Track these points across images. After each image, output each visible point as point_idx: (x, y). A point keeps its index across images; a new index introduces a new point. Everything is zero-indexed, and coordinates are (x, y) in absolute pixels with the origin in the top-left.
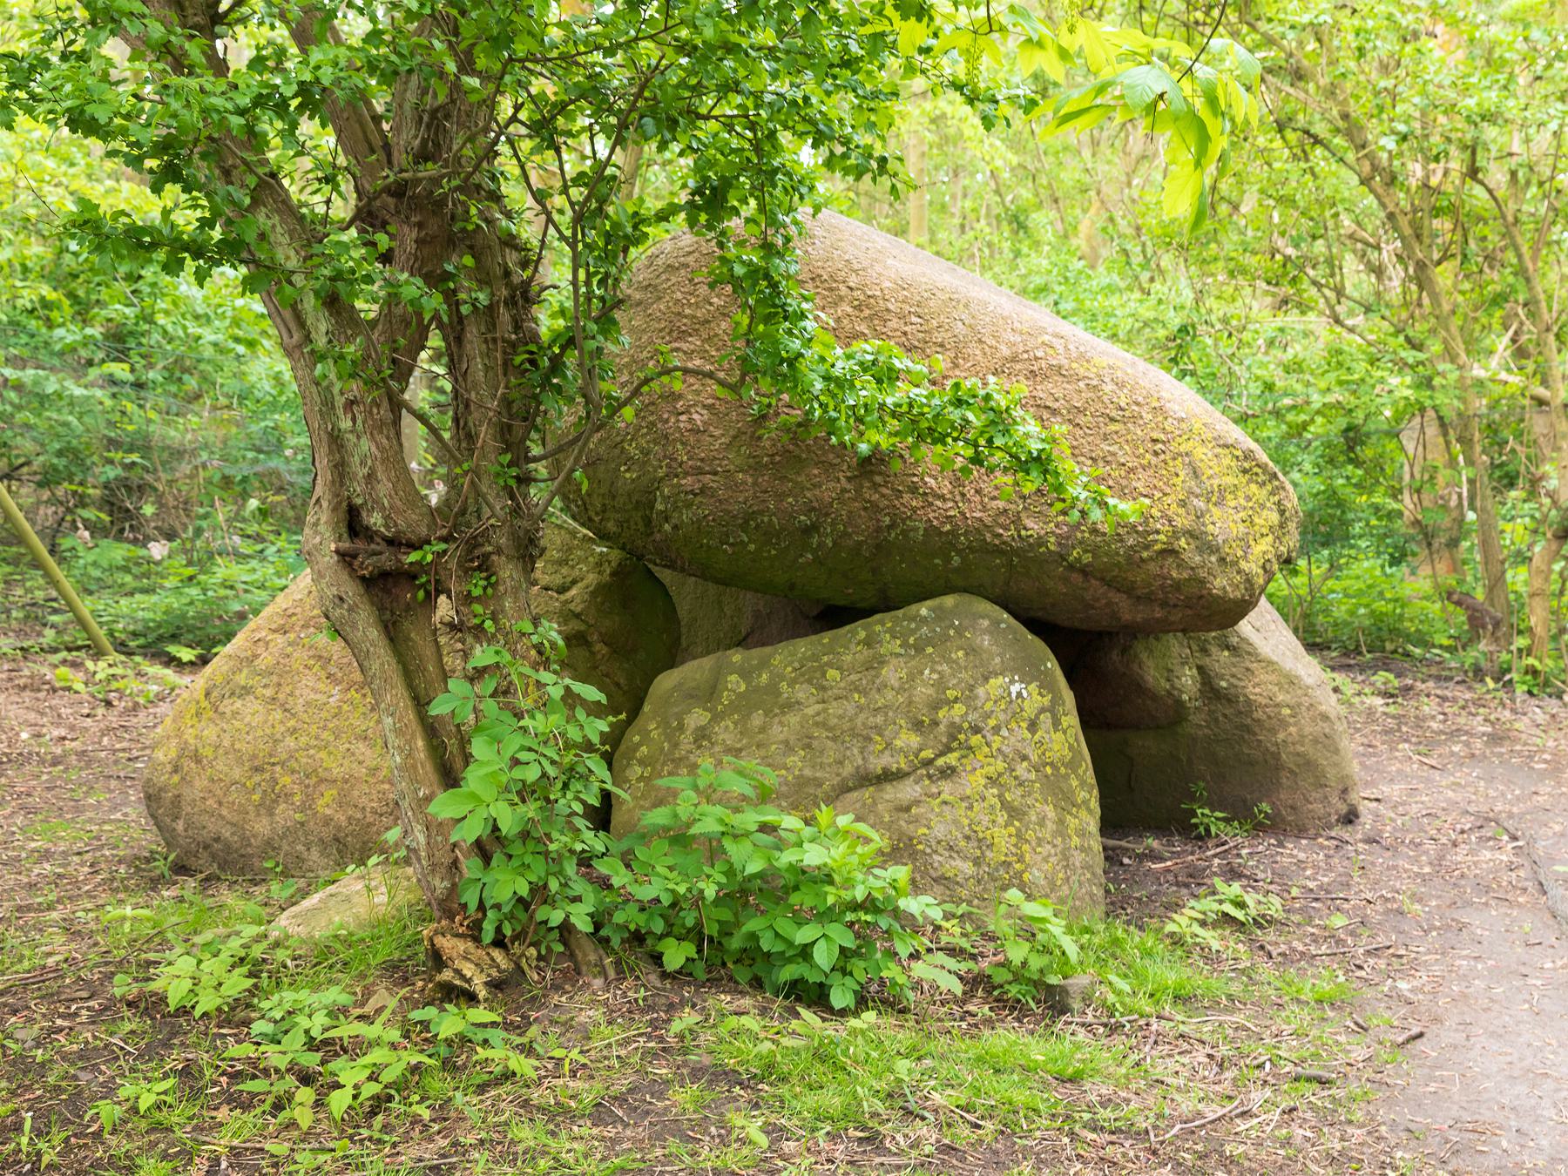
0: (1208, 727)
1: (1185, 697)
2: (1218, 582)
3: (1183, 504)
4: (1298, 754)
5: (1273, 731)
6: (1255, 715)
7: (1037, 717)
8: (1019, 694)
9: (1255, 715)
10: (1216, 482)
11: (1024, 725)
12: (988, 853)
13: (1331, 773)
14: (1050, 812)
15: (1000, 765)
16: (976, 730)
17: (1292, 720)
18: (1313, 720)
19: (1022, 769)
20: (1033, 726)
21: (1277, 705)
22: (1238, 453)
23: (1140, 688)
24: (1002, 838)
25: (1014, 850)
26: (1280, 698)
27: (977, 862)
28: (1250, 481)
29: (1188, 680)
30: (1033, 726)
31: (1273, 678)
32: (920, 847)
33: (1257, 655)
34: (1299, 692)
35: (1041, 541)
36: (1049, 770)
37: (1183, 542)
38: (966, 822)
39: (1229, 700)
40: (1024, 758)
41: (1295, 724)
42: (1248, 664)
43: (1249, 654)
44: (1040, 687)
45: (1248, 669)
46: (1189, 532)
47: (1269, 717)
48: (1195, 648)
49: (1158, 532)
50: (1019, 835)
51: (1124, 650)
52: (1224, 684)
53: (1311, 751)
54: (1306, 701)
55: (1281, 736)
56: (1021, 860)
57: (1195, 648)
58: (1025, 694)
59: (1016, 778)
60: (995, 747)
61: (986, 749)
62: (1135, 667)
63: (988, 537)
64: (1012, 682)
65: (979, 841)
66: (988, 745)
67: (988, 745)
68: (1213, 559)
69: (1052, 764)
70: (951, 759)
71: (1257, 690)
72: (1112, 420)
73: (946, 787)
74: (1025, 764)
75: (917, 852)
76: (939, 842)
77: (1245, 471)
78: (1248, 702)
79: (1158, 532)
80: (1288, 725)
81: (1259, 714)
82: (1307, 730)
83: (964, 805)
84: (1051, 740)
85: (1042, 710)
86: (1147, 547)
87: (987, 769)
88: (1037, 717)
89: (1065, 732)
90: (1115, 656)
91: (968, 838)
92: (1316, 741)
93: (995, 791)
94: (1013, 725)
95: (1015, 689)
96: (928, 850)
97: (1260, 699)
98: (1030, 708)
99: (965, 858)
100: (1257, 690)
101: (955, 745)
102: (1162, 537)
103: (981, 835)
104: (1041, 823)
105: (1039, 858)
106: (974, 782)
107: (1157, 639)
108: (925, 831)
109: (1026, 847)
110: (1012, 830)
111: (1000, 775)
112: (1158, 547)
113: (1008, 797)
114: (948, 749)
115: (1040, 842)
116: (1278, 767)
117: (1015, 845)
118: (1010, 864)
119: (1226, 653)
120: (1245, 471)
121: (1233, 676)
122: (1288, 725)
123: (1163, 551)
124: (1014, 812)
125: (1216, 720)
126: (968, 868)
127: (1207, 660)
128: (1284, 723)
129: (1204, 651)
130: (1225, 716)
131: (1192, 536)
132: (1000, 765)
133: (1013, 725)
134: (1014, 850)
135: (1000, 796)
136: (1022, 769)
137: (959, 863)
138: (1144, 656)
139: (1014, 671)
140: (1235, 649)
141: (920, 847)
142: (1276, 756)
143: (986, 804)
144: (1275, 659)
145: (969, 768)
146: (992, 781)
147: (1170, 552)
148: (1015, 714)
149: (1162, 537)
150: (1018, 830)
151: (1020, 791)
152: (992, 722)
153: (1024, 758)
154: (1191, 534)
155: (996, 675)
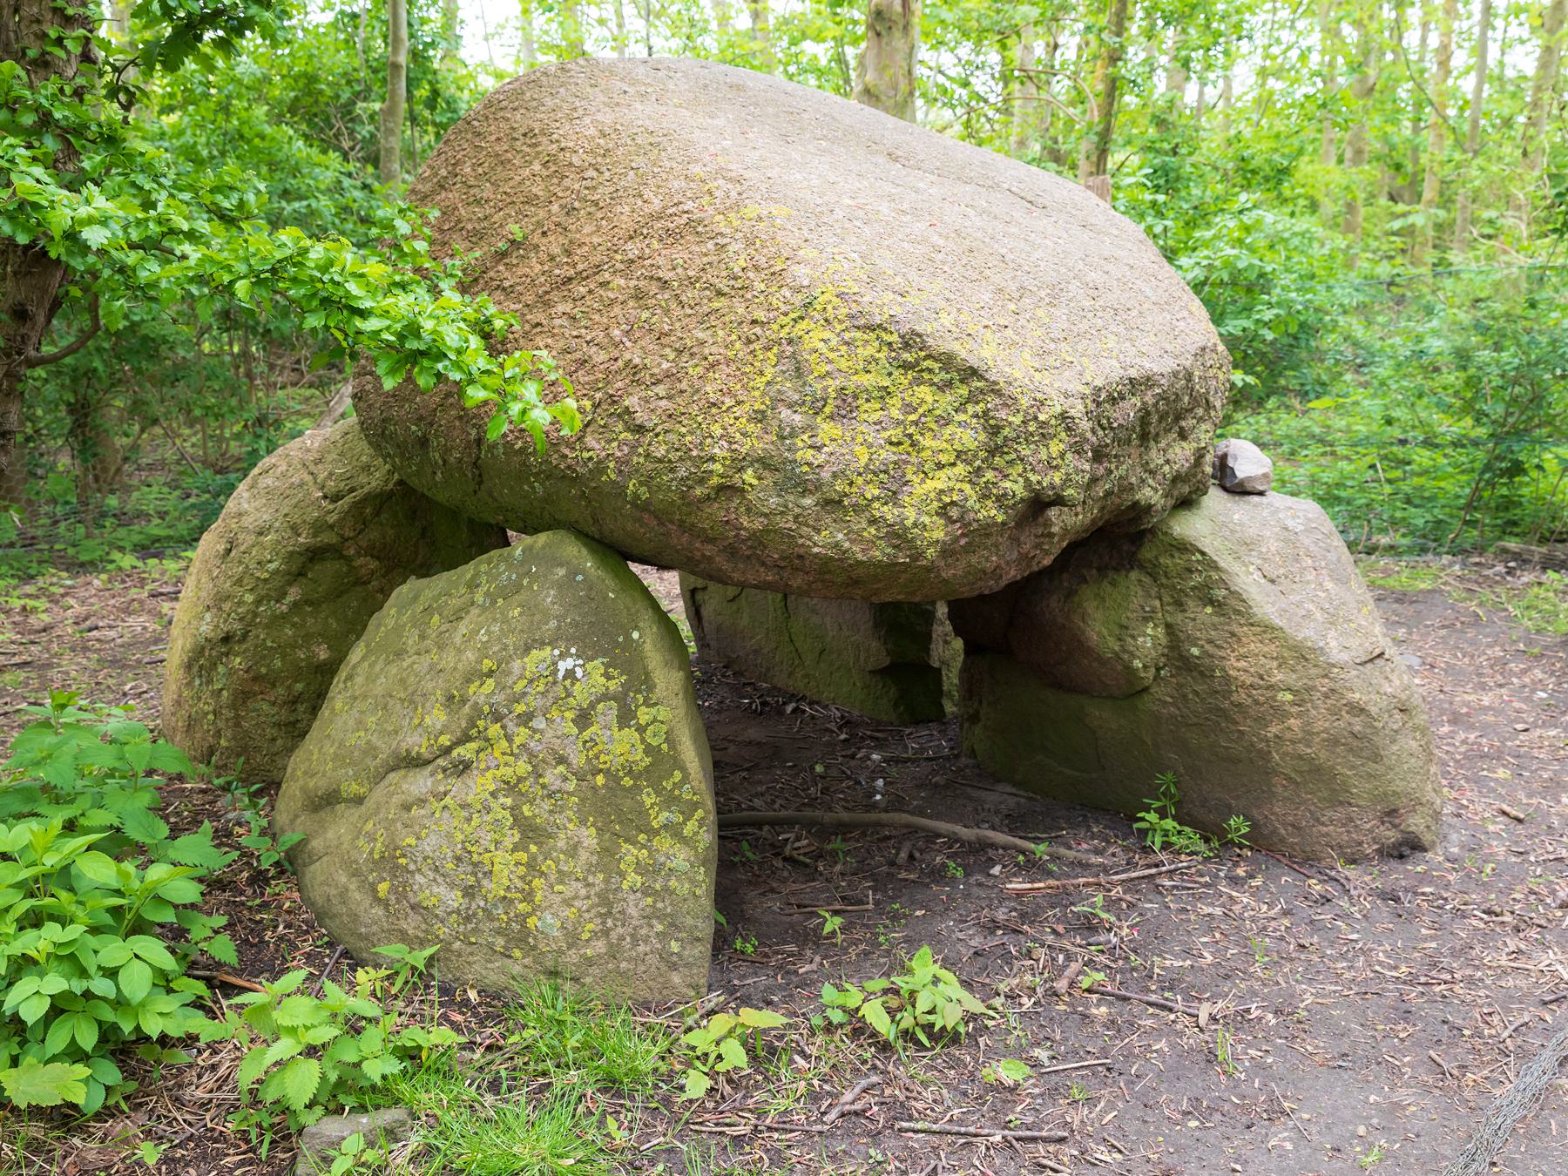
0: (1174, 704)
1: (1138, 664)
2: (822, 538)
3: (760, 417)
4: (1300, 757)
5: (1262, 721)
6: (1235, 697)
7: (592, 706)
8: (570, 674)
9: (1235, 697)
10: (833, 385)
11: (569, 715)
12: (485, 882)
13: (1360, 788)
14: (589, 837)
15: (523, 767)
16: (498, 718)
17: (1295, 709)
18: (1335, 712)
19: (552, 776)
20: (584, 719)
21: (1270, 687)
22: (894, 338)
23: (1080, 646)
24: (505, 867)
25: (520, 884)
26: (1278, 677)
27: (469, 892)
28: (918, 382)
29: (1148, 641)
30: (584, 719)
31: (1271, 649)
32: (402, 861)
33: (1251, 616)
34: (1314, 671)
35: (600, 468)
36: (600, 780)
37: (749, 476)
38: (460, 837)
39: (1202, 673)
40: (562, 760)
41: (1299, 715)
42: (1236, 629)
43: (1238, 612)
44: (607, 666)
45: (1233, 634)
46: (760, 460)
47: (1256, 702)
48: (1167, 599)
49: (712, 459)
50: (532, 865)
51: (1071, 593)
52: (1195, 651)
53: (1323, 755)
54: (1324, 685)
55: (1274, 729)
56: (528, 896)
57: (1167, 599)
58: (579, 673)
59: (544, 786)
60: (518, 741)
61: (504, 744)
62: (1076, 619)
63: (555, 459)
64: (562, 656)
65: (475, 865)
66: (509, 739)
67: (509, 739)
68: (808, 501)
69: (607, 772)
70: (465, 751)
71: (1242, 664)
72: (720, 293)
73: (455, 785)
74: (561, 768)
75: (397, 866)
76: (425, 859)
77: (907, 366)
78: (1227, 679)
79: (712, 459)
80: (1286, 715)
81: (1241, 697)
82: (1320, 725)
83: (464, 814)
84: (611, 740)
85: (605, 697)
86: (702, 481)
87: (503, 770)
88: (592, 706)
89: (641, 730)
90: (1054, 602)
91: (459, 859)
92: (1334, 742)
93: (509, 801)
94: (555, 714)
95: (563, 666)
96: (412, 867)
97: (1243, 677)
98: (581, 694)
99: (452, 886)
100: (1242, 664)
101: (473, 732)
102: (717, 467)
103: (475, 857)
104: (573, 851)
105: (558, 899)
106: (480, 785)
107: (1113, 584)
108: (413, 842)
109: (537, 882)
110: (523, 856)
111: (520, 780)
112: (715, 481)
113: (526, 810)
114: (465, 739)
115: (562, 877)
116: (1269, 772)
117: (522, 878)
118: (511, 901)
119: (1209, 610)
120: (907, 366)
121: (1210, 642)
122: (1286, 715)
123: (721, 489)
124: (530, 832)
125: (1185, 696)
126: (455, 899)
127: (1180, 616)
128: (1281, 713)
129: (1179, 605)
130: (1196, 693)
131: (766, 466)
132: (523, 767)
133: (555, 714)
134: (520, 884)
135: (514, 810)
136: (552, 776)
137: (441, 890)
138: (1090, 606)
139: (571, 640)
140: (1220, 605)
141: (402, 861)
142: (1265, 756)
143: (488, 818)
144: (1278, 622)
145: (483, 766)
146: (510, 787)
147: (728, 490)
148: (557, 700)
149: (717, 467)
150: (533, 858)
151: (547, 805)
152: (520, 708)
153: (562, 760)
154: (764, 463)
155: (542, 644)
